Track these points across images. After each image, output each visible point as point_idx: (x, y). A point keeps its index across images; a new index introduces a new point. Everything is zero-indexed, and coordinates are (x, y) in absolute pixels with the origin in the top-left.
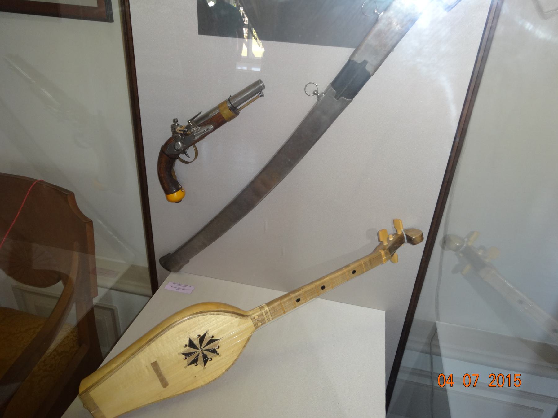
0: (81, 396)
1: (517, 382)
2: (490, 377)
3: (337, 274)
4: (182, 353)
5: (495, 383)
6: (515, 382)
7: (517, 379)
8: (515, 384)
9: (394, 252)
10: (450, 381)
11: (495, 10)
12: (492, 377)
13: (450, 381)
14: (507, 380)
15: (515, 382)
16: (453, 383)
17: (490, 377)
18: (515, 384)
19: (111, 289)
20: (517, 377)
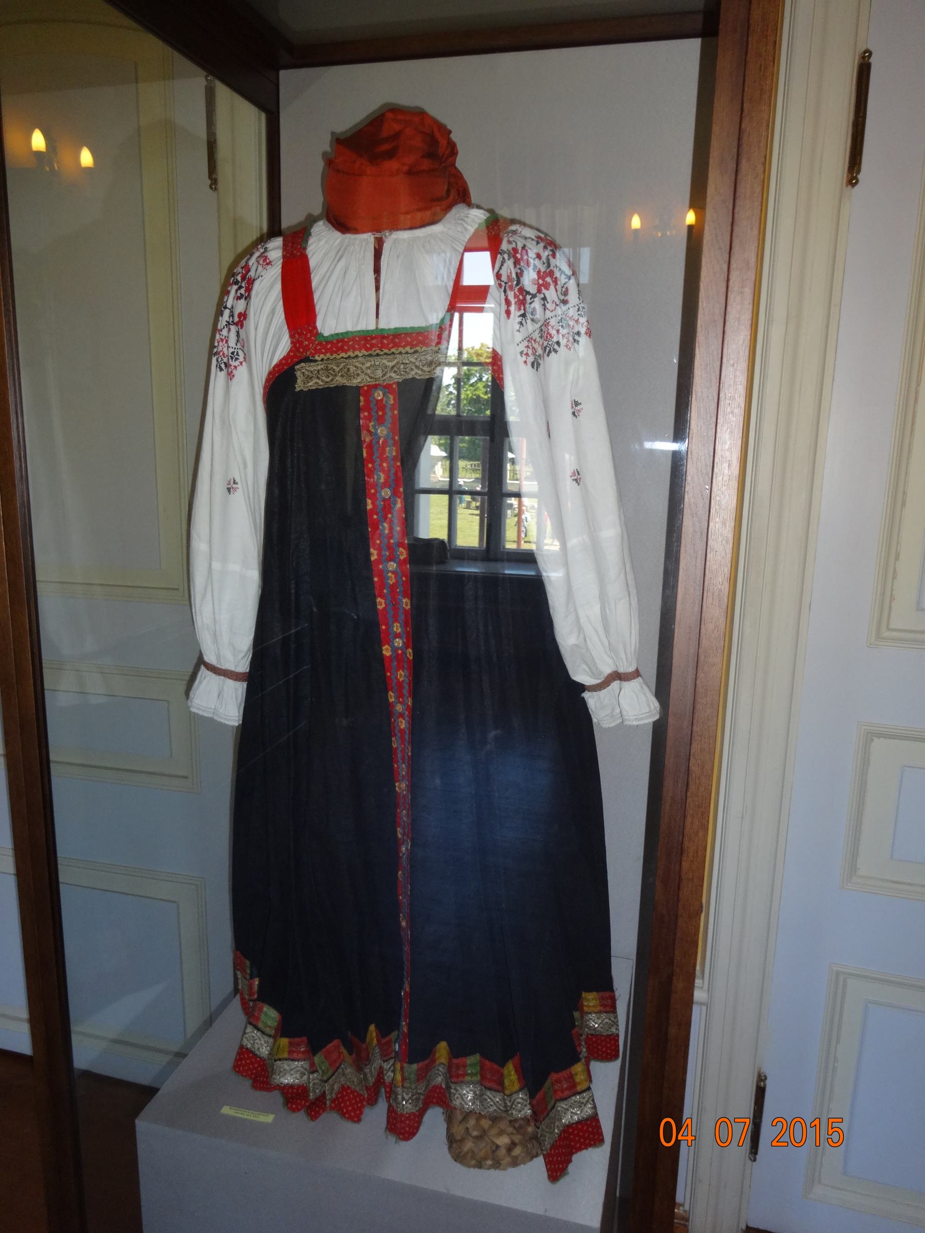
0: (701, 985)
1: (835, 1137)
2: (774, 1124)
3: (262, 330)
4: (762, 1071)
5: (786, 1138)
6: (830, 1137)
7: (834, 1130)
8: (830, 1140)
9: (681, 517)
10: (685, 1134)
11: (143, 770)
12: (798, 1124)
13: (685, 1134)
14: (811, 1132)
15: (830, 1137)
16: (693, 1138)
17: (774, 1124)
18: (830, 1140)
19: (115, 1041)
20: (834, 1125)
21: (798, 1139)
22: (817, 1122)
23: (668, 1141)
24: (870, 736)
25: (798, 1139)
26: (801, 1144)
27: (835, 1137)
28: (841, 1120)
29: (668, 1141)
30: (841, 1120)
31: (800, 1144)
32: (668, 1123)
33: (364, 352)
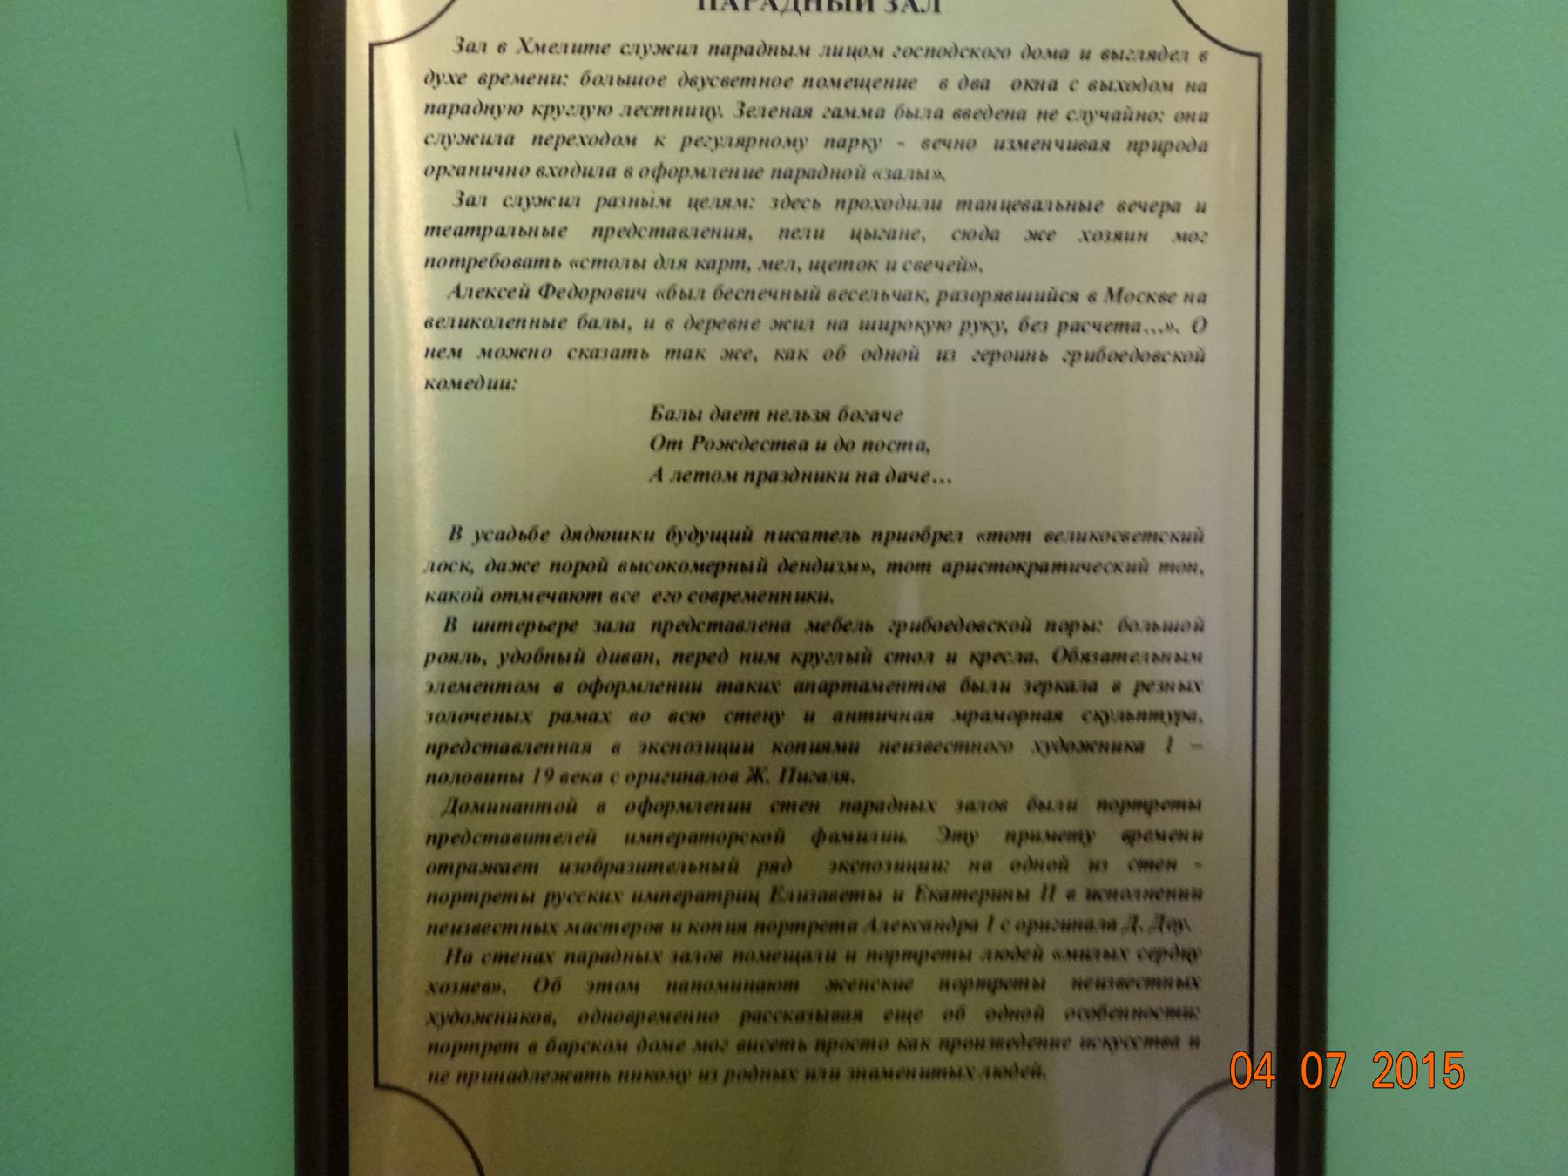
1: (1454, 1076)
2: (1376, 1060)
5: (1391, 1078)
7: (1452, 1067)
8: (1447, 1081)
14: (1423, 1069)
17: (1376, 1060)
20: (1453, 1061)
21: (1406, 1078)
22: (1430, 1057)
23: (1312, 1081)
24: (1259, 56)
25: (1406, 1078)
26: (1411, 1085)
27: (1454, 1076)
28: (1461, 1055)
29: (1312, 1081)
30: (1461, 1055)
31: (1410, 1085)
32: (1312, 1059)
33: (849, 598)
